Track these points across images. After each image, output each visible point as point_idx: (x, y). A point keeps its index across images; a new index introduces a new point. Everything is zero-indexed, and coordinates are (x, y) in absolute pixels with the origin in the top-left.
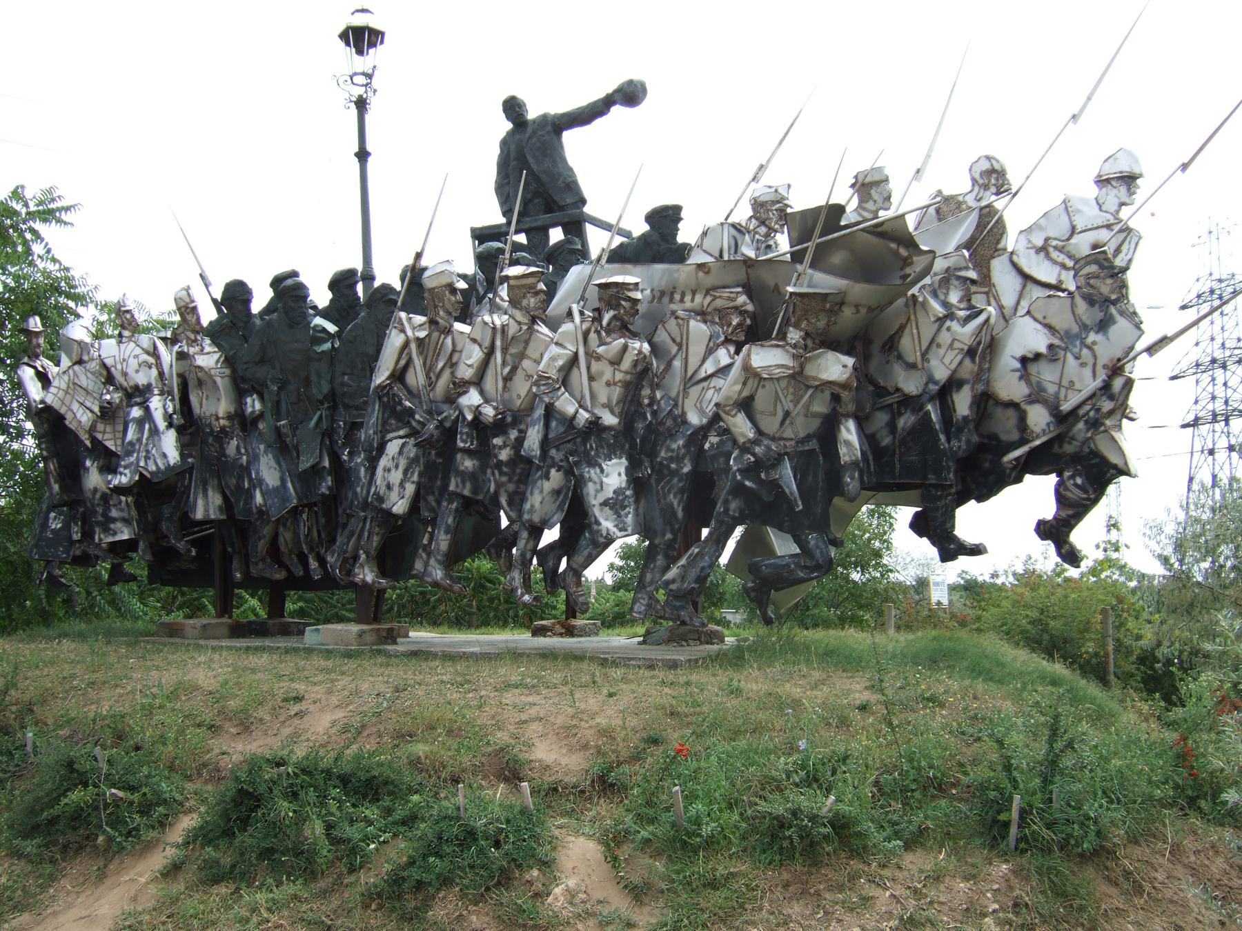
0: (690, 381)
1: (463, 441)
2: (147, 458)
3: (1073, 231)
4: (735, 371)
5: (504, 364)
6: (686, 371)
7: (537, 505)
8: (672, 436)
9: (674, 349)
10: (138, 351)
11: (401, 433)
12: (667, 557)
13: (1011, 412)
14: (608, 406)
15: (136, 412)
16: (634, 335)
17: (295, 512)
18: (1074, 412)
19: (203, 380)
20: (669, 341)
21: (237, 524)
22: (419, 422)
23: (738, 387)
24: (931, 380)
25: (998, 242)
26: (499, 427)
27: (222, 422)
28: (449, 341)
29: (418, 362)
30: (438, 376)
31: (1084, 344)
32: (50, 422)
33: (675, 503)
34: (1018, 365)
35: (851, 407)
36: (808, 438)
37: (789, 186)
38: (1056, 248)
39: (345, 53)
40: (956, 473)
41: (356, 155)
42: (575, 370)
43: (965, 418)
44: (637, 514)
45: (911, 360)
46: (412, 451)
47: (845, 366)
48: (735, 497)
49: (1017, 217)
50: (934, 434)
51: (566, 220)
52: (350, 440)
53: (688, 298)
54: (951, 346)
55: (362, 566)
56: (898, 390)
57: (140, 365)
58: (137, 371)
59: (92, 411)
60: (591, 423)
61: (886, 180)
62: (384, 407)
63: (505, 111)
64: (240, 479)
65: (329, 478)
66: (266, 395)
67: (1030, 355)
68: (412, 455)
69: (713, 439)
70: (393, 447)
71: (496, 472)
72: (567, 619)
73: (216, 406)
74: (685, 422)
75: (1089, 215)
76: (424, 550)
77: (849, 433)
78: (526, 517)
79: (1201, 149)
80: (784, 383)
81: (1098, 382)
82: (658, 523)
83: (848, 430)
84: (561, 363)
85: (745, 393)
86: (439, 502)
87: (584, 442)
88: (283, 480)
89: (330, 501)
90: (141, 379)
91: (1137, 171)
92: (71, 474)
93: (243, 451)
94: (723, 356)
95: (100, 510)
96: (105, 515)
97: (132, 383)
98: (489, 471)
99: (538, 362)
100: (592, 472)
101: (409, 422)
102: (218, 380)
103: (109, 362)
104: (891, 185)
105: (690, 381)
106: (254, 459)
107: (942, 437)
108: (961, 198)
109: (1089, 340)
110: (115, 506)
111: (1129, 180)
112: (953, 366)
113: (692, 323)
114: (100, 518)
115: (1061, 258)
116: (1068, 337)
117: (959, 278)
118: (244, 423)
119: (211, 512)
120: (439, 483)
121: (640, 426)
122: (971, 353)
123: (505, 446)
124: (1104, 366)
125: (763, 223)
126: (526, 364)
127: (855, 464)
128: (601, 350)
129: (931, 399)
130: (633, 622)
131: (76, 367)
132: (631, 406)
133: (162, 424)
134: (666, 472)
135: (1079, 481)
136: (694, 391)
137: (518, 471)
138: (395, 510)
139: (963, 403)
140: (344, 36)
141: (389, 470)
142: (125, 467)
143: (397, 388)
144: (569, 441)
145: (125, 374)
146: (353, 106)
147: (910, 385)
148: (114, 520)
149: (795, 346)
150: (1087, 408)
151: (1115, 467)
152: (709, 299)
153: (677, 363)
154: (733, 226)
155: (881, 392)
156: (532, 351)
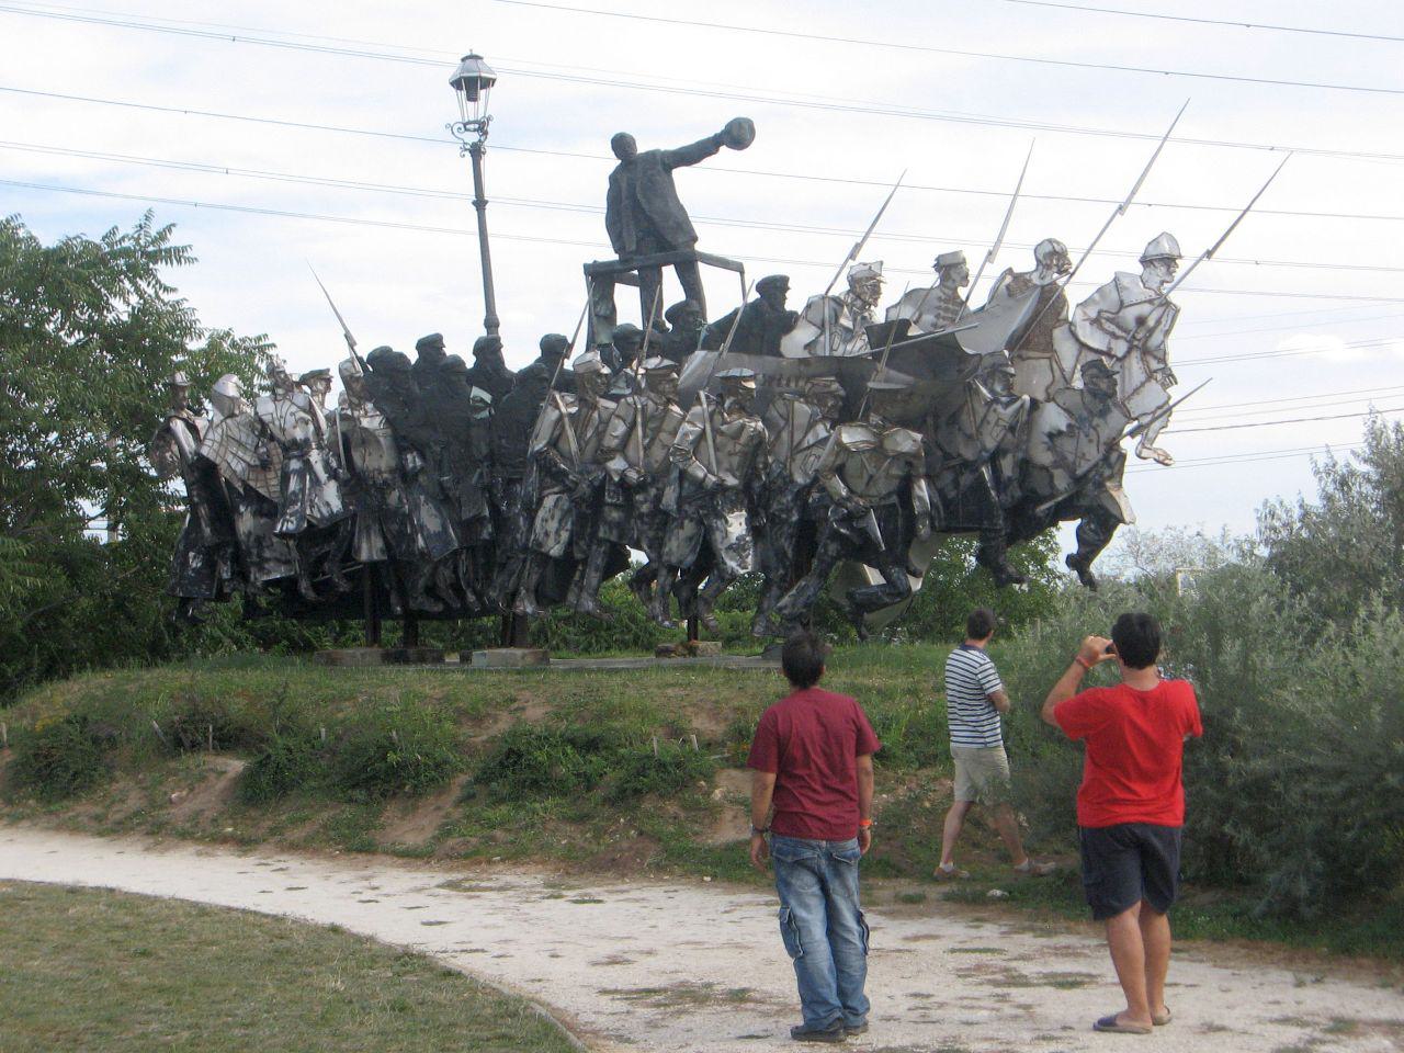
0: (796, 449)
1: (610, 497)
2: (312, 507)
3: (1122, 305)
4: (832, 439)
5: (644, 436)
6: (792, 442)
7: (674, 549)
8: (781, 491)
9: (782, 423)
10: (294, 409)
11: (556, 489)
12: (780, 588)
13: (1044, 473)
14: (730, 470)
15: (295, 465)
16: (750, 416)
17: (455, 553)
18: (1085, 475)
19: (367, 438)
20: (776, 414)
21: (399, 564)
22: (572, 481)
23: (832, 459)
24: (984, 449)
25: (1059, 314)
26: (642, 487)
27: (385, 475)
28: (596, 415)
29: (570, 432)
30: (587, 443)
31: (1090, 425)
32: (203, 473)
33: (786, 545)
34: (1046, 439)
35: (922, 470)
36: (889, 495)
37: (882, 263)
38: (1108, 320)
39: (455, 97)
40: (1005, 519)
41: (474, 203)
42: (703, 443)
43: (1010, 479)
44: (755, 556)
45: (968, 432)
46: (565, 503)
47: (914, 441)
48: (832, 541)
49: (1076, 292)
50: (986, 490)
51: (678, 260)
52: (510, 496)
53: (793, 385)
54: (997, 424)
55: (523, 600)
56: (959, 455)
57: (297, 422)
58: (295, 427)
59: (244, 461)
60: (718, 485)
61: (964, 261)
62: (540, 468)
63: (614, 148)
64: (403, 524)
65: (490, 526)
66: (428, 454)
67: (1054, 432)
68: (565, 507)
69: (815, 495)
70: (549, 502)
71: (639, 522)
72: (689, 639)
73: (378, 461)
74: (792, 481)
75: (1138, 292)
76: (576, 585)
77: (922, 490)
78: (665, 558)
79: (1222, 240)
80: (867, 455)
81: (1100, 456)
82: (773, 561)
83: (920, 488)
84: (691, 438)
85: (839, 462)
86: (589, 546)
87: (712, 499)
88: (444, 527)
89: (489, 549)
90: (299, 434)
91: (1175, 253)
92: (224, 516)
93: (405, 501)
94: (821, 431)
95: (255, 551)
96: (259, 556)
97: (289, 438)
98: (633, 521)
99: (674, 433)
100: (719, 523)
101: (563, 482)
102: (382, 439)
103: (267, 419)
104: (967, 266)
105: (796, 449)
106: (416, 507)
107: (993, 493)
108: (1027, 277)
109: (1094, 423)
110: (268, 547)
111: (1169, 261)
112: (999, 439)
113: (796, 404)
114: (255, 559)
115: (1112, 328)
116: (1080, 420)
117: (1002, 372)
118: (406, 477)
119: (374, 553)
120: (589, 530)
121: (756, 485)
122: (1012, 429)
123: (646, 501)
124: (1105, 444)
125: (858, 297)
126: (663, 436)
127: (927, 514)
128: (724, 428)
129: (984, 462)
130: (753, 641)
131: (229, 421)
132: (749, 472)
133: (323, 476)
134: (777, 521)
135: (1092, 526)
136: (800, 457)
137: (657, 521)
138: (552, 552)
139: (1007, 466)
140: (452, 84)
141: (547, 521)
142: (291, 515)
143: (553, 453)
144: (699, 499)
145: (283, 430)
146: (468, 154)
147: (968, 453)
148: (268, 560)
149: (875, 426)
150: (1094, 473)
151: (1115, 517)
152: (809, 385)
153: (785, 435)
154: (836, 300)
155: (947, 456)
156: (668, 425)
